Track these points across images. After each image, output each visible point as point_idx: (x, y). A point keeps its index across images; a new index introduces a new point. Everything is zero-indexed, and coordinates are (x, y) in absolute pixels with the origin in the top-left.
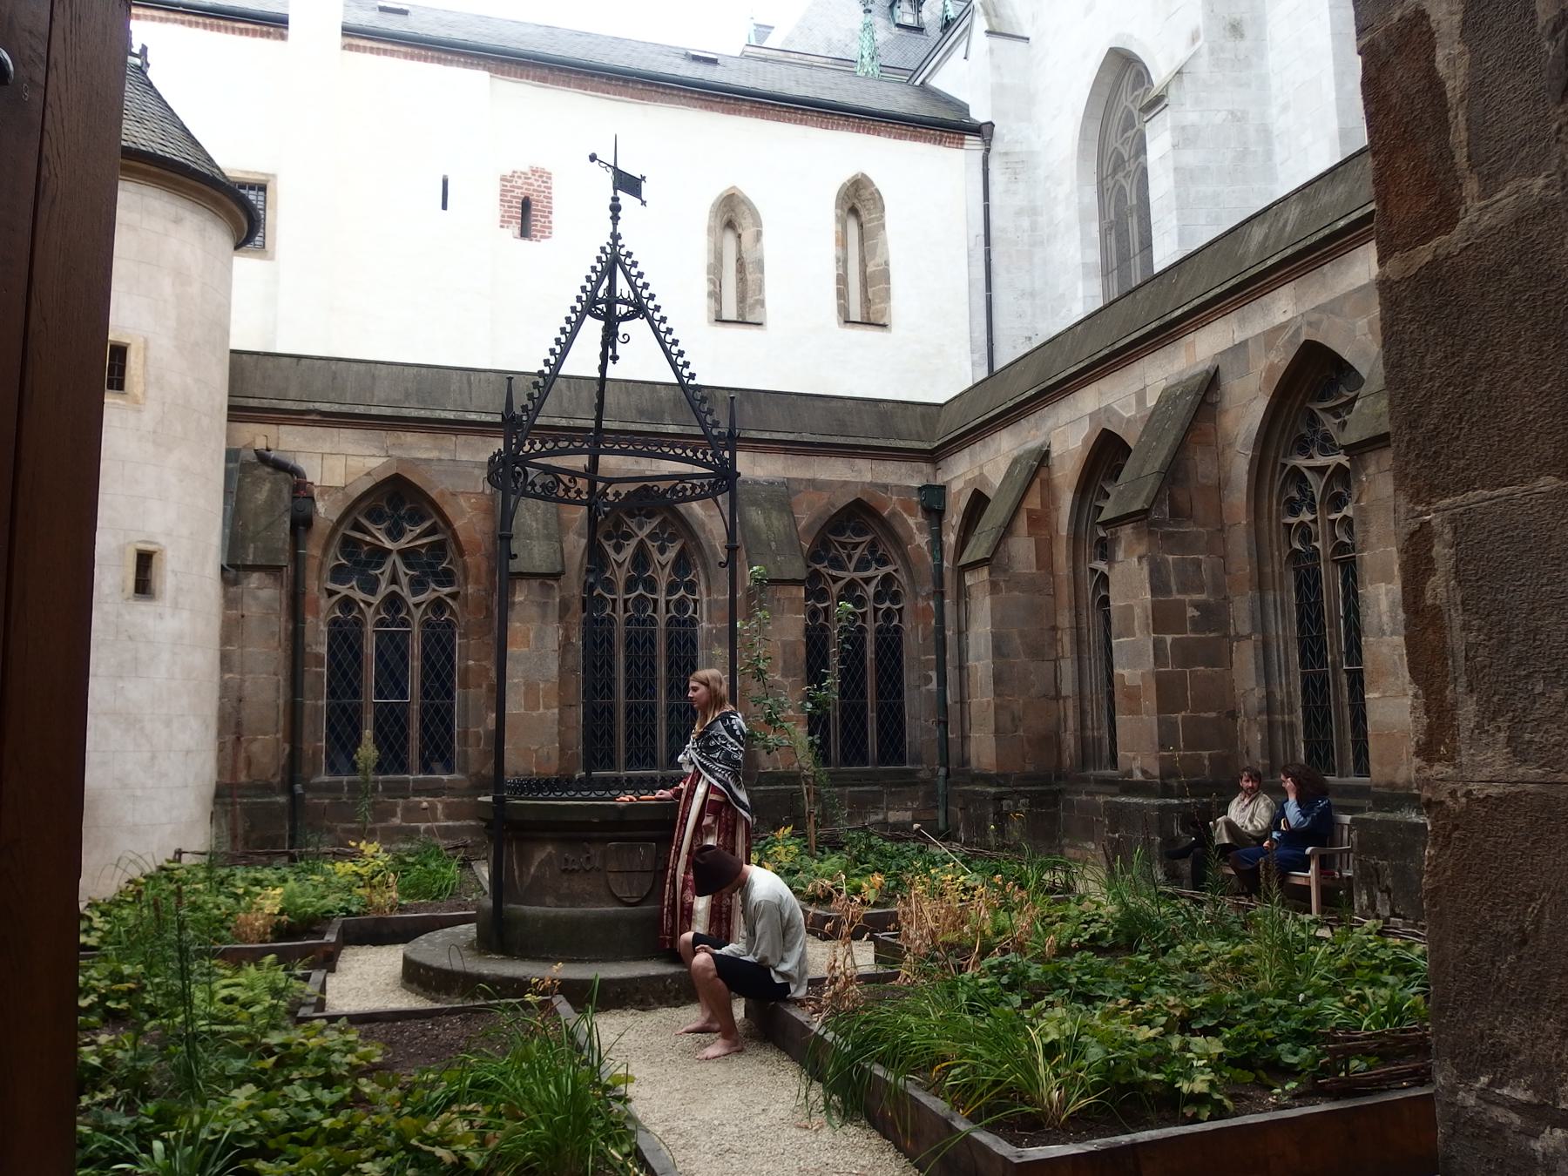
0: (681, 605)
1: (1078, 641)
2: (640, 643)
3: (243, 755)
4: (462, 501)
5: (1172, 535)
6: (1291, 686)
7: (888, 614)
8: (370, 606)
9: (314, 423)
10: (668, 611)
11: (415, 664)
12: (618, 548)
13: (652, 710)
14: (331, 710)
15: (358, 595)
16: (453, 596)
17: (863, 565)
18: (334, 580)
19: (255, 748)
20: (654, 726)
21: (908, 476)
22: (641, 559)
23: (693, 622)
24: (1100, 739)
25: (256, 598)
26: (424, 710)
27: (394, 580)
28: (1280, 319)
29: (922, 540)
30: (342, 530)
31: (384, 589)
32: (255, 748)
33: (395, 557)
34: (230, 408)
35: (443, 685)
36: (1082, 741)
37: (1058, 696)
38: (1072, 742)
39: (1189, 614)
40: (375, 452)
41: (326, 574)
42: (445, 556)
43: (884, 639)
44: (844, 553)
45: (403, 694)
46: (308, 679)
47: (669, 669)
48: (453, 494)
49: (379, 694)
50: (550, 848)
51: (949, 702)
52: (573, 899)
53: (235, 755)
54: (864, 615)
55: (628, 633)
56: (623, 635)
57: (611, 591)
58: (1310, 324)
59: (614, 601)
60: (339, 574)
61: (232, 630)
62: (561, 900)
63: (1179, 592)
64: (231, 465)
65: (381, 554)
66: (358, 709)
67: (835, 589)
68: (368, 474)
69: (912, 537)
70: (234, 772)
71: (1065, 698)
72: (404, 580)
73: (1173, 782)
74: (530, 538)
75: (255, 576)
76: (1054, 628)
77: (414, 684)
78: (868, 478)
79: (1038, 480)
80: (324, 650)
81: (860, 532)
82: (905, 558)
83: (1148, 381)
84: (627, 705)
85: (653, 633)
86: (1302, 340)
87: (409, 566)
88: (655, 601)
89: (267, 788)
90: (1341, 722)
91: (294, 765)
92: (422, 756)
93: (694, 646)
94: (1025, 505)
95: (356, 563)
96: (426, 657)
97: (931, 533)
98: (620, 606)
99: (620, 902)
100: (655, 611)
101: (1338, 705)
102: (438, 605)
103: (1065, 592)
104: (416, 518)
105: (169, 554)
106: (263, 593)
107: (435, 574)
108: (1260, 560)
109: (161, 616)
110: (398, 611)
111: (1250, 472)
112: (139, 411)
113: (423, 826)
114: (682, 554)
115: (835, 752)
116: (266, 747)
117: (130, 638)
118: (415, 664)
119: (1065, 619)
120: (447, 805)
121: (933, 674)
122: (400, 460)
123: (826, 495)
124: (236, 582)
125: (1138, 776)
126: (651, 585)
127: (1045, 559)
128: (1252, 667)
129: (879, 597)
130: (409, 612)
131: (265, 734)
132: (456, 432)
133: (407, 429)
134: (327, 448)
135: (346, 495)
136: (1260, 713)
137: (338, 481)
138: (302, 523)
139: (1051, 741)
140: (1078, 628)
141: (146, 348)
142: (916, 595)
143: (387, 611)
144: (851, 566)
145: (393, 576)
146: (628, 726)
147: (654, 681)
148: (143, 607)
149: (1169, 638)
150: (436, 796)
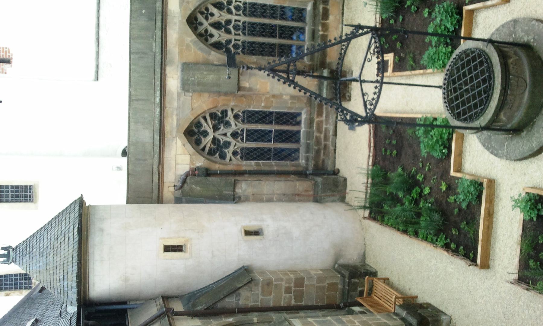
2: (252, 29)
3: (303, 193)
4: (195, 106)
8: (236, 145)
9: (163, 168)
11: (260, 127)
12: (212, 36)
13: (282, 27)
14: (275, 159)
15: (232, 148)
16: (232, 110)
19: (301, 189)
22: (217, 26)
25: (246, 190)
26: (277, 123)
27: (225, 135)
30: (206, 156)
31: (229, 139)
32: (301, 189)
33: (217, 135)
34: (158, 203)
35: (267, 115)
40: (174, 143)
41: (223, 161)
42: (215, 113)
45: (270, 132)
46: (267, 168)
48: (192, 109)
49: (270, 141)
53: (303, 195)
55: (249, 35)
59: (235, 40)
60: (223, 156)
61: (258, 199)
64: (184, 200)
65: (215, 141)
66: (275, 149)
68: (184, 145)
70: (309, 196)
72: (225, 131)
74: (220, 78)
75: (237, 190)
77: (267, 127)
80: (253, 162)
88: (236, 21)
89: (316, 184)
91: (301, 174)
92: (294, 125)
95: (218, 149)
96: (257, 122)
98: (237, 37)
99: (525, 91)
100: (240, 21)
102: (236, 117)
104: (198, 125)
105: (244, 224)
106: (244, 187)
107: (223, 117)
109: (268, 225)
110: (237, 133)
112: (191, 239)
113: (324, 126)
116: (301, 186)
117: (278, 236)
118: (260, 127)
120: (317, 117)
122: (178, 131)
124: (240, 198)
126: (228, 22)
130: (238, 129)
131: (296, 186)
132: (164, 107)
133: (164, 128)
134: (173, 162)
135: (194, 154)
137: (188, 157)
138: (208, 173)
141: (164, 238)
143: (238, 137)
145: (224, 134)
147: (270, 25)
148: (266, 232)
150: (314, 121)
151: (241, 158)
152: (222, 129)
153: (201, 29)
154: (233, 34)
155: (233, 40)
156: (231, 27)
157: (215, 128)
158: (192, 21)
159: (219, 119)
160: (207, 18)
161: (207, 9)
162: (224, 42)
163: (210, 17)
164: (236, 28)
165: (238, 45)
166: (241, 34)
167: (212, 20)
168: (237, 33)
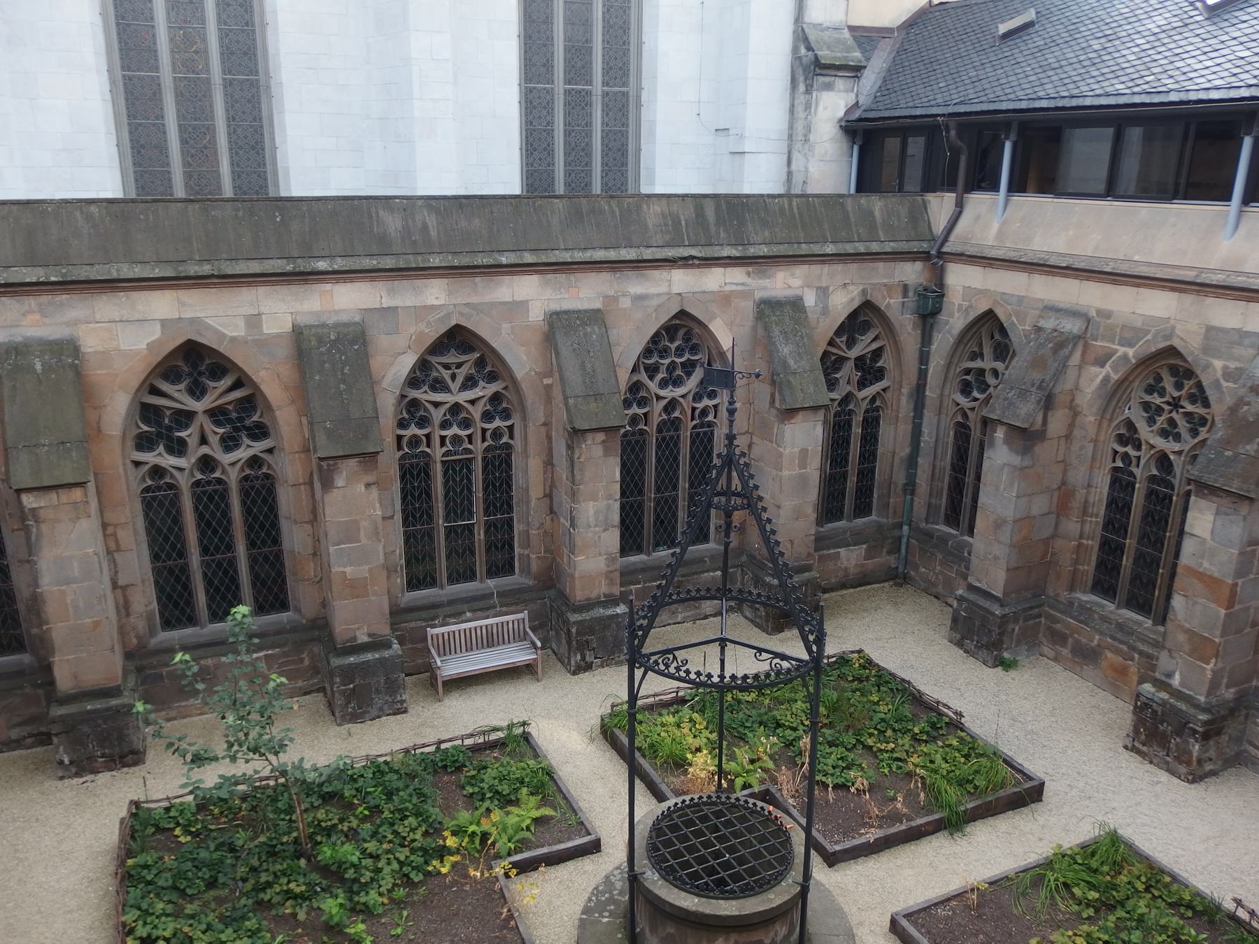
9: (699, 266)
15: (169, 461)
16: (270, 451)
17: (470, 382)
18: (139, 447)
27: (204, 441)
43: (664, 439)
44: (446, 374)
47: (485, 489)
60: (144, 443)
65: (185, 418)
67: (437, 415)
72: (214, 440)
83: (263, 309)
86: (453, 323)
87: (218, 423)
102: (255, 462)
125: (365, 639)
129: (487, 416)
143: (152, 479)
144: (454, 386)
145: (204, 438)
151: (197, 484)
152: (216, 432)
157: (217, 414)
158: (458, 338)
159: (169, 429)
163: (844, 339)
166: (486, 444)
168: (488, 434)
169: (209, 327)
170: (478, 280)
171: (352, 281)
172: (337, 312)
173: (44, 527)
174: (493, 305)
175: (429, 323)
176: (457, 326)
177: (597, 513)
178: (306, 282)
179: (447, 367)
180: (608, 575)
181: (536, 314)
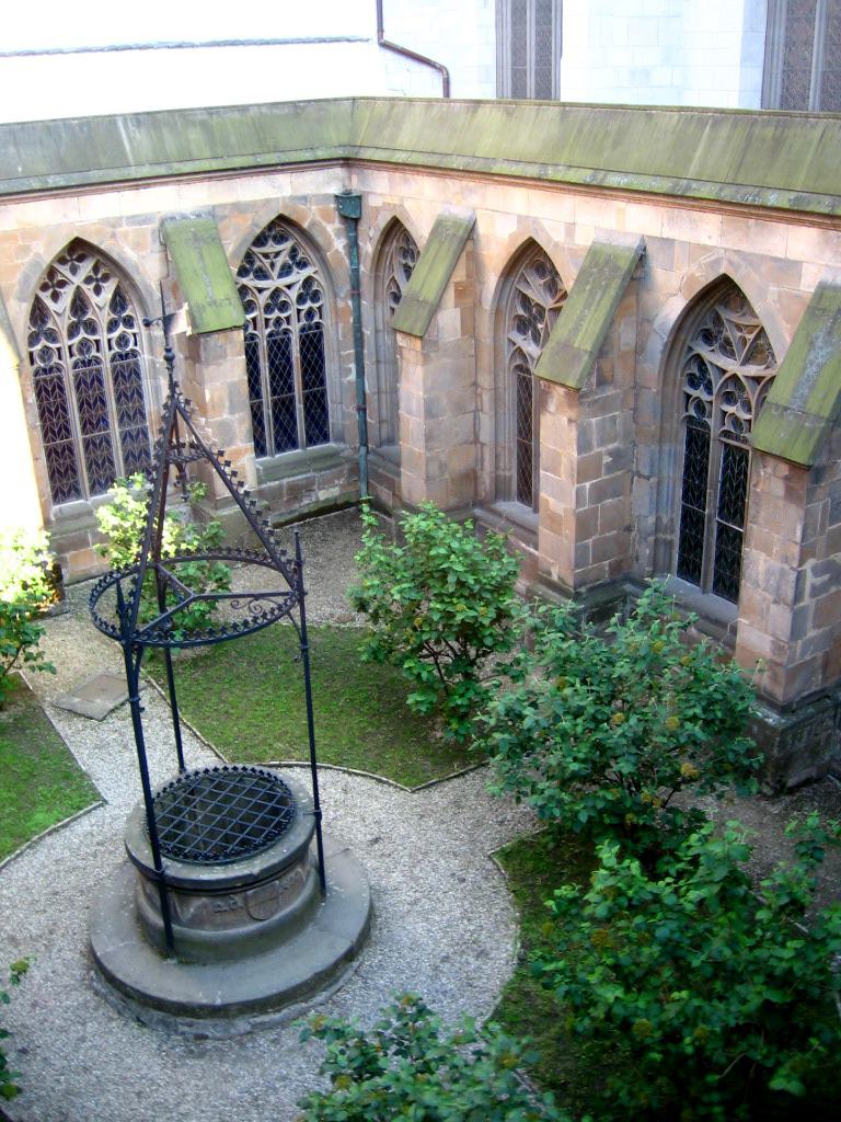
0: (122, 340)
1: (496, 400)
2: (89, 383)
5: (596, 401)
6: (673, 515)
7: (310, 314)
10: (110, 348)
17: (286, 271)
20: (64, 401)
21: (328, 183)
22: (79, 305)
23: (134, 354)
24: (510, 478)
28: (704, 241)
29: (339, 244)
36: (497, 480)
37: (476, 440)
38: (488, 482)
39: (604, 462)
44: (267, 262)
50: (204, 900)
51: (367, 390)
52: (225, 926)
54: (288, 319)
55: (76, 376)
56: (72, 378)
57: (54, 340)
58: (730, 262)
59: (59, 349)
62: (217, 926)
63: (599, 446)
69: (330, 243)
71: (483, 445)
73: (583, 590)
76: (475, 384)
78: (288, 192)
79: (464, 254)
81: (280, 239)
82: (324, 262)
83: (578, 220)
84: (85, 440)
85: (99, 371)
86: (722, 271)
88: (97, 342)
90: (708, 558)
93: (138, 375)
94: (453, 280)
97: (348, 237)
101: (709, 545)
103: (486, 358)
108: (664, 417)
111: (663, 352)
114: (118, 293)
115: (270, 443)
119: (485, 380)
121: (353, 366)
123: (250, 216)
126: (91, 327)
127: (469, 327)
128: (647, 500)
129: (301, 299)
136: (650, 535)
139: (471, 477)
140: (496, 389)
142: (335, 295)
144: (275, 274)
146: (87, 459)
149: (588, 485)
153: (65, 270)
154: (70, 343)
155: (58, 345)
156: (44, 342)
158: (79, 249)
160: (88, 280)
161: (106, 278)
162: (50, 325)
164: (84, 345)
165: (50, 358)
167: (88, 289)
169: (543, 230)
170: (752, 222)
171: (639, 201)
172: (626, 234)
173: (404, 362)
174: (763, 258)
175: (700, 266)
176: (724, 275)
177: (769, 572)
178: (605, 197)
179: (266, 256)
180: (773, 664)
181: (808, 284)
